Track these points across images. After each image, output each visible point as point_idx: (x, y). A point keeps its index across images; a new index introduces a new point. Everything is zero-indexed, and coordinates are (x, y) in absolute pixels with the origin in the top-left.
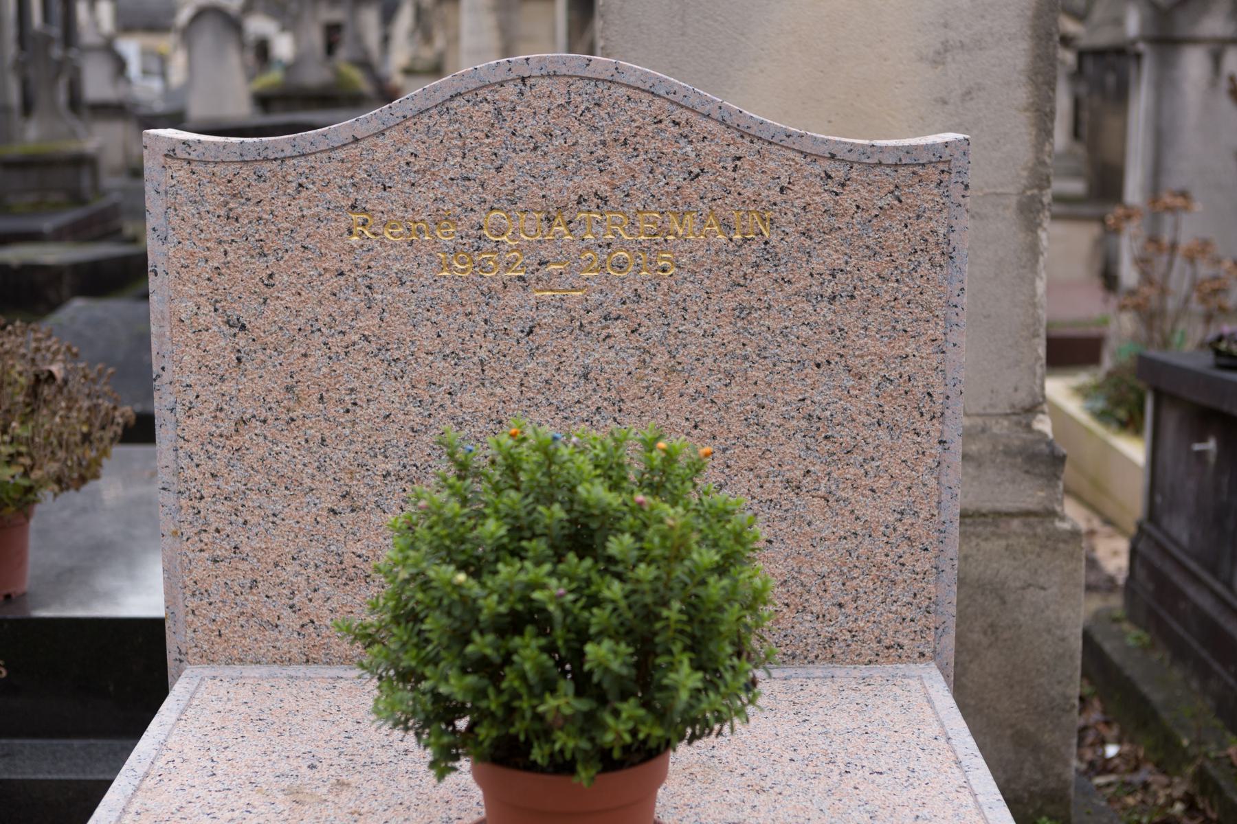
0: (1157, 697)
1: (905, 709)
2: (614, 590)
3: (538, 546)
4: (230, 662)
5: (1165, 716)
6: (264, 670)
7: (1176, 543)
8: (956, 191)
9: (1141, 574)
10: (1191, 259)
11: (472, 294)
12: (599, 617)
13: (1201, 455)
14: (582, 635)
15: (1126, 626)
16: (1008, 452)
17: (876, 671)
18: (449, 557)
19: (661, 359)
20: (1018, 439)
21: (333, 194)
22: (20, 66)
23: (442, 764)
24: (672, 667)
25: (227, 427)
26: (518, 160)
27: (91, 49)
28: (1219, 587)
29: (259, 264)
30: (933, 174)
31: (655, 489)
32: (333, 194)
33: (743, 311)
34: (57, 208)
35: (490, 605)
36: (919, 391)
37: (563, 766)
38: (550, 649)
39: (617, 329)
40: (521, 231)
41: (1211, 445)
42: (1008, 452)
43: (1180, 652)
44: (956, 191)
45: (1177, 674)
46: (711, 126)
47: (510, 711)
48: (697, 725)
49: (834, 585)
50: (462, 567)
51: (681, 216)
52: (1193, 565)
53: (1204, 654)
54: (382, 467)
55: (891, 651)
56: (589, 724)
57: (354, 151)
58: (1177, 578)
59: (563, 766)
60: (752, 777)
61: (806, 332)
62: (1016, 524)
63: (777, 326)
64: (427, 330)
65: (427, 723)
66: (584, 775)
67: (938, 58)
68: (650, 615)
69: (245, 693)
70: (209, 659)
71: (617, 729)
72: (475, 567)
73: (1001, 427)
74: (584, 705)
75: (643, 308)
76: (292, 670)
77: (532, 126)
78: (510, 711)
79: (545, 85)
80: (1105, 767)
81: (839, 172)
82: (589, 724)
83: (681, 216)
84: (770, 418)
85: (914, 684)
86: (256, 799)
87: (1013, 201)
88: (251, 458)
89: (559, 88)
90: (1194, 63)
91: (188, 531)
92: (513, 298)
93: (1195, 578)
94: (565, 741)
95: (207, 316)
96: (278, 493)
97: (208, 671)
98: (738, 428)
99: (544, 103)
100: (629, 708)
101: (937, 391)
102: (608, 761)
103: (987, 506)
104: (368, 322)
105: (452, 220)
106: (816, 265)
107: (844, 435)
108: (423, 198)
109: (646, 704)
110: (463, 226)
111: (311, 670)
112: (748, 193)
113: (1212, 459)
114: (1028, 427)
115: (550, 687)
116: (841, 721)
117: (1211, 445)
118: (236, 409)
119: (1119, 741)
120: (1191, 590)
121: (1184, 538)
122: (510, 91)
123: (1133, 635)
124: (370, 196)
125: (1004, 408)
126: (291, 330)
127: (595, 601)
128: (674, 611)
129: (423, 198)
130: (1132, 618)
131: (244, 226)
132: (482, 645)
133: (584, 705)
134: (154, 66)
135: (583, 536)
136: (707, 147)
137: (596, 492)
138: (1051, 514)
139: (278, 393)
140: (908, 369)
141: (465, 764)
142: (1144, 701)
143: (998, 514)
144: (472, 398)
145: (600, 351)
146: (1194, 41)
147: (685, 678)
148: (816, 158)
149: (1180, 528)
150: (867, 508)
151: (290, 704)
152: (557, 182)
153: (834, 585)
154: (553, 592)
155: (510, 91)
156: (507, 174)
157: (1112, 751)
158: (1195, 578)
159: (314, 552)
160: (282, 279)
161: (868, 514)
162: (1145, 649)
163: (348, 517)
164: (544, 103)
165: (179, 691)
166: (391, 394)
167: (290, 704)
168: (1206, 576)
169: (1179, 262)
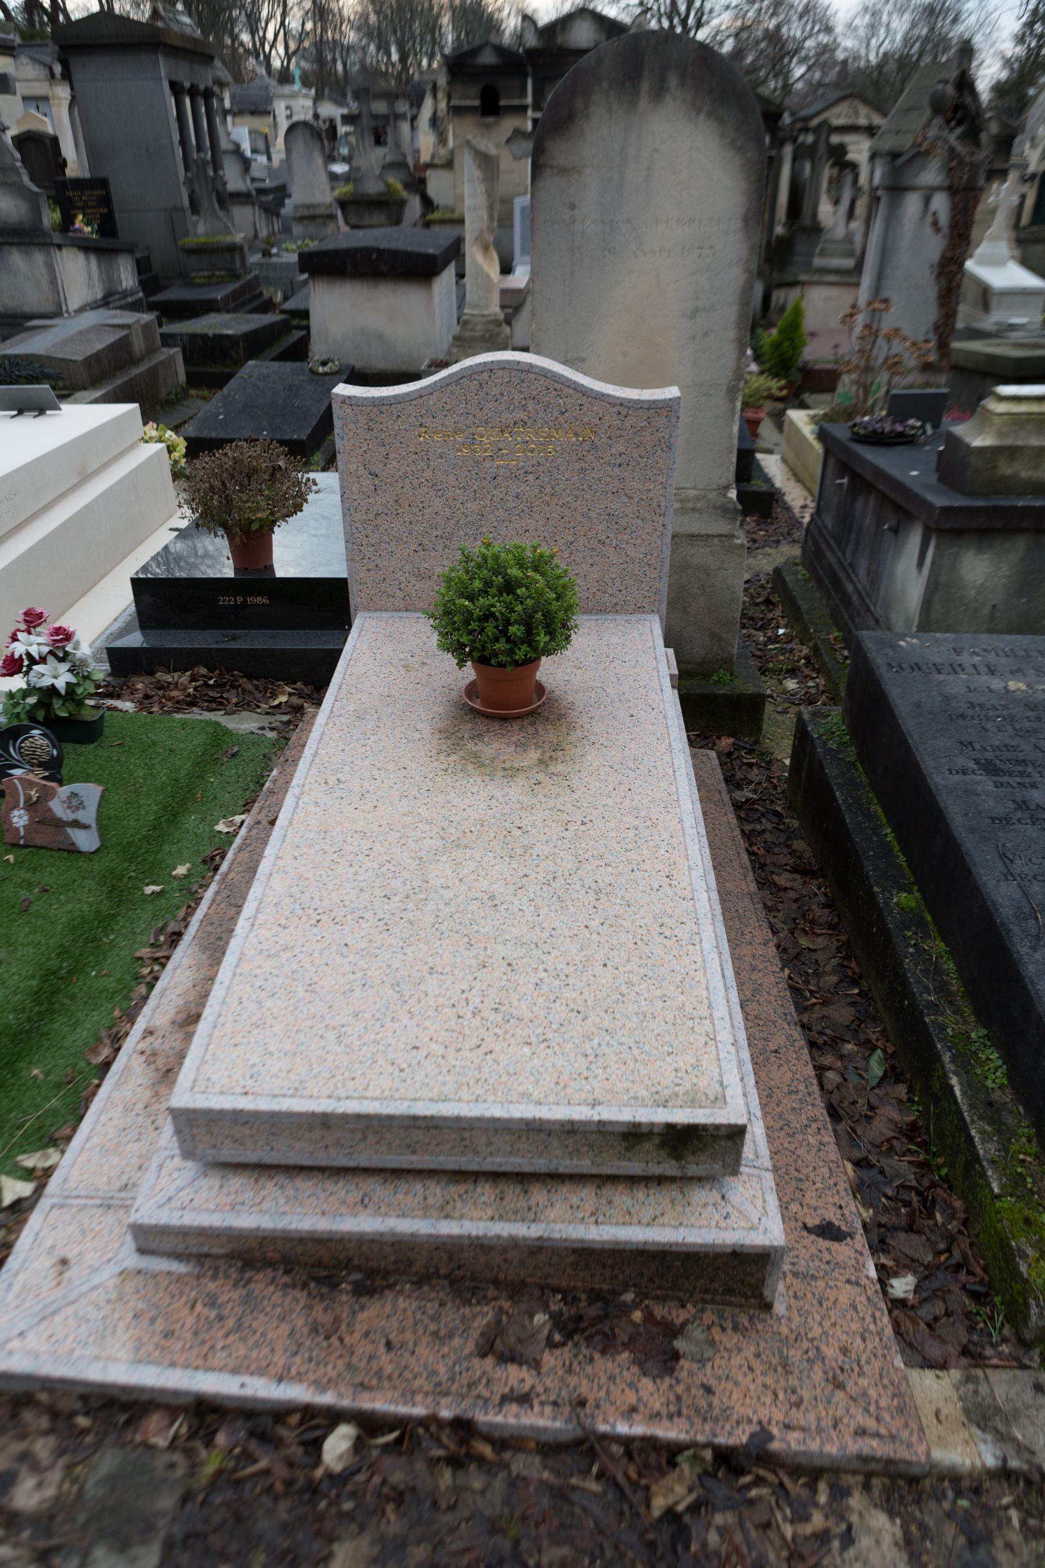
0: (804, 606)
1: (641, 635)
2: (519, 608)
3: (493, 591)
4: (375, 610)
5: (806, 617)
6: (389, 614)
7: (826, 527)
8: (674, 420)
9: (810, 541)
10: (888, 339)
11: (471, 462)
12: (514, 616)
13: (841, 484)
14: (508, 622)
15: (800, 568)
16: (714, 507)
17: (634, 617)
18: (462, 595)
19: (548, 490)
20: (720, 501)
21: (412, 420)
22: (189, 182)
23: (461, 664)
24: (538, 634)
25: (371, 516)
26: (489, 405)
27: (226, 152)
28: (840, 554)
29: (382, 449)
30: (664, 412)
31: (536, 569)
32: (412, 420)
33: (582, 470)
34: (222, 282)
35: (477, 612)
36: (655, 504)
37: (502, 665)
38: (496, 627)
39: (531, 477)
40: (489, 438)
41: (845, 481)
42: (714, 507)
43: (820, 585)
44: (674, 420)
45: (818, 595)
46: (571, 391)
47: (484, 647)
48: (548, 652)
49: (618, 583)
50: (467, 598)
51: (557, 430)
52: (831, 541)
53: (830, 587)
54: (435, 533)
55: (640, 609)
56: (511, 652)
57: (420, 401)
58: (823, 546)
59: (502, 665)
60: (577, 663)
61: (608, 479)
62: (716, 540)
63: (597, 477)
64: (452, 477)
65: (456, 650)
66: (509, 669)
67: (693, 315)
68: (531, 617)
69: (383, 624)
70: (367, 609)
71: (521, 652)
72: (471, 598)
73: (712, 496)
74: (508, 646)
75: (541, 469)
76: (400, 614)
77: (495, 391)
78: (484, 647)
79: (500, 373)
80: (776, 639)
81: (624, 411)
82: (511, 652)
83: (557, 430)
84: (593, 515)
85: (647, 623)
86: (392, 669)
87: (725, 387)
88: (381, 529)
89: (506, 374)
90: (912, 203)
91: (357, 558)
92: (487, 464)
93: (832, 549)
94: (502, 658)
95: (361, 471)
96: (393, 543)
97: (367, 615)
98: (579, 518)
99: (500, 381)
100: (524, 647)
101: (663, 504)
102: (516, 664)
103: (703, 532)
104: (428, 474)
105: (462, 431)
106: (613, 451)
107: (623, 522)
108: (449, 421)
109: (530, 646)
110: (467, 434)
111: (408, 614)
112: (586, 420)
113: (845, 487)
114: (725, 495)
115: (497, 640)
116: (615, 640)
117: (845, 481)
118: (375, 509)
119: (786, 627)
120: (828, 554)
121: (830, 526)
122: (486, 375)
123: (802, 572)
124: (428, 421)
125: (714, 486)
126: (396, 477)
127: (513, 611)
128: (539, 615)
129: (449, 421)
130: (803, 564)
131: (375, 433)
132: (474, 625)
133: (508, 646)
134: (261, 146)
135: (509, 587)
136: (569, 400)
137: (514, 572)
138: (733, 536)
139: (392, 503)
140: (651, 495)
141: (469, 663)
142: (798, 608)
143: (709, 536)
144: (472, 506)
145: (523, 487)
146: (914, 189)
147: (543, 638)
148: (614, 405)
149: (829, 520)
150: (632, 553)
151: (401, 629)
152: (505, 415)
153: (618, 583)
154: (499, 608)
155: (486, 375)
156: (485, 412)
157: (781, 631)
158: (832, 549)
159: (408, 567)
160: (392, 456)
161: (632, 554)
162: (805, 580)
163: (421, 553)
164: (500, 381)
165: (357, 623)
166: (438, 504)
167: (401, 629)
168: (835, 548)
169: (881, 341)
